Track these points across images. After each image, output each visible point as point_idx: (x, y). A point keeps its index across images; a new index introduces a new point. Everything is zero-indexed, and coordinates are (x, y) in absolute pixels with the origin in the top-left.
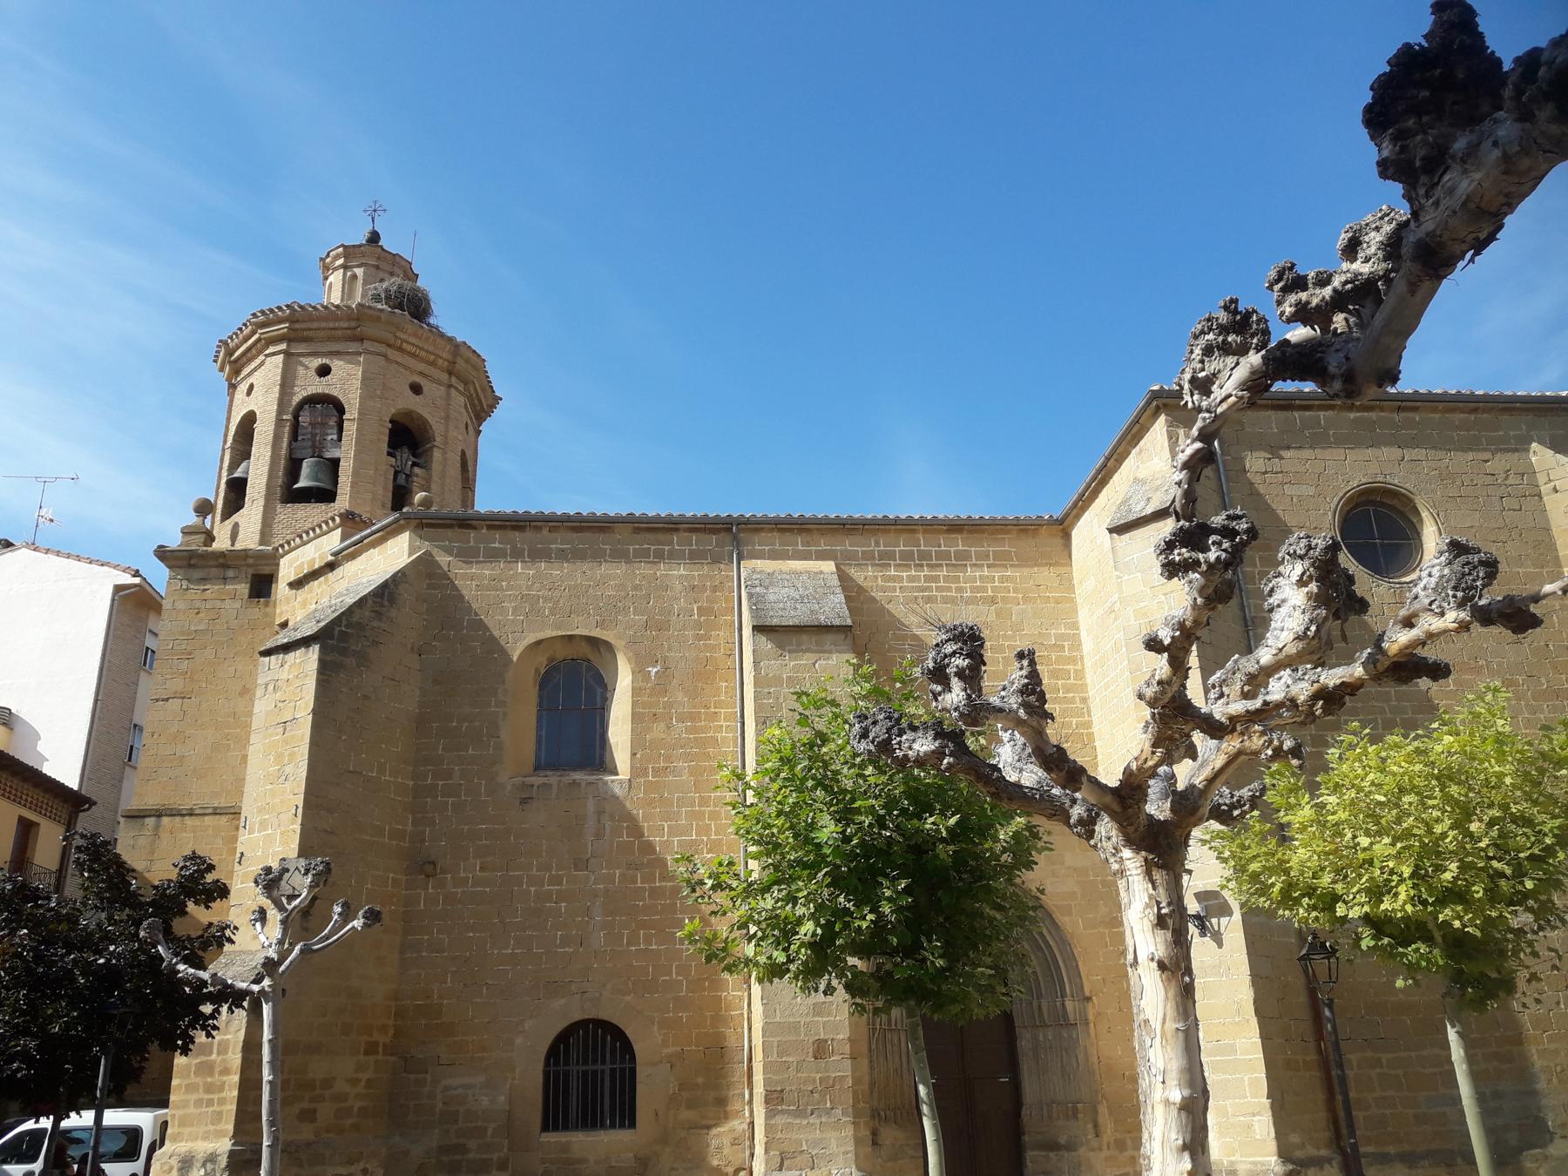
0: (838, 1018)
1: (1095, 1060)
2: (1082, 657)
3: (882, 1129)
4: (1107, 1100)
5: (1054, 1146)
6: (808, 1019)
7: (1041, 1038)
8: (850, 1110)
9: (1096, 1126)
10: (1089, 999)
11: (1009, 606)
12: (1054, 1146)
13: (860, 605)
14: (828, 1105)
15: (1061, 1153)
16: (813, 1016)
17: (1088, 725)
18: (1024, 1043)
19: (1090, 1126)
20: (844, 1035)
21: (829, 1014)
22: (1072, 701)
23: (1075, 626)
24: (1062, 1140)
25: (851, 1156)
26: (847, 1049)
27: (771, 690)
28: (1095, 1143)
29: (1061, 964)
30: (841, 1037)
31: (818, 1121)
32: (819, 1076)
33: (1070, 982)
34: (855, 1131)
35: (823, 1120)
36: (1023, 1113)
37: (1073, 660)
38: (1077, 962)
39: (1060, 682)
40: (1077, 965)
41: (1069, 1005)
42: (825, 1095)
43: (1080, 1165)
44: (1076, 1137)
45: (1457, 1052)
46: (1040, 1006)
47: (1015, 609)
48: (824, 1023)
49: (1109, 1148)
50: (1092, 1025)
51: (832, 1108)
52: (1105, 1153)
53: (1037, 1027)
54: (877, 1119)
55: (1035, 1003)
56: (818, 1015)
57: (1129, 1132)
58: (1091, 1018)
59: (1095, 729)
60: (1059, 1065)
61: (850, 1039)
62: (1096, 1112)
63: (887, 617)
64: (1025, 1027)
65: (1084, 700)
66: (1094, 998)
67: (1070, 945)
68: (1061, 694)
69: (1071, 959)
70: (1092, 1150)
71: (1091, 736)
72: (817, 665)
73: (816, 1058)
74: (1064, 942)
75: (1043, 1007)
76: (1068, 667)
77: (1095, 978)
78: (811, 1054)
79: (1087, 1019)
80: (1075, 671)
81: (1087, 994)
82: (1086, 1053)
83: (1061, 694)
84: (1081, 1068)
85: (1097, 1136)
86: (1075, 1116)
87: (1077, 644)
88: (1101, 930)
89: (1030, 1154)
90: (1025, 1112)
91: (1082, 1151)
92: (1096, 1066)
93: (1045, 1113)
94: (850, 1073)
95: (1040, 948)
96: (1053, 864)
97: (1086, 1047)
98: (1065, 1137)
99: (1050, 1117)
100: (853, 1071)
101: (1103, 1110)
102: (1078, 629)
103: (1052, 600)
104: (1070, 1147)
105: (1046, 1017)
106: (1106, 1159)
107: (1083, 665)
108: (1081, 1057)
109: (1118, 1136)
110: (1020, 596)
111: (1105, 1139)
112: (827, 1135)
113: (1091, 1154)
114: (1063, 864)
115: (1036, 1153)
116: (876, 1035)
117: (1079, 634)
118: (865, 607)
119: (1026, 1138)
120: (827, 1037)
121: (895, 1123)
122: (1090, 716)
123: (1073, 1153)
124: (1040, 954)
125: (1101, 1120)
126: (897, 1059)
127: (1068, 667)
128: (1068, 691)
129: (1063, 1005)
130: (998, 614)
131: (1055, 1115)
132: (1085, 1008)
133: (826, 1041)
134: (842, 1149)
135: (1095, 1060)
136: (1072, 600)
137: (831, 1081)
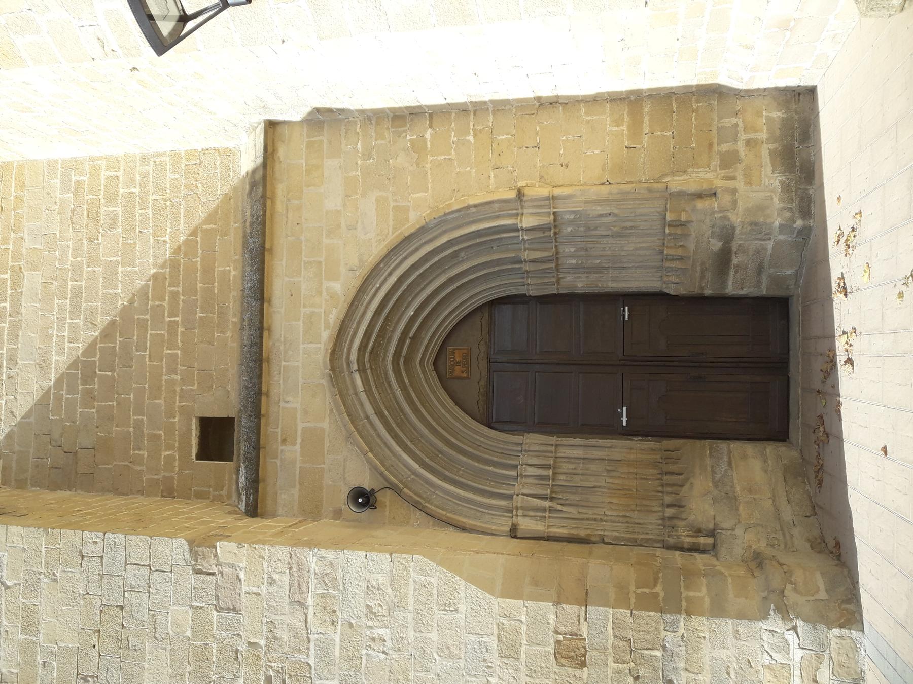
0: (523, 619)
1: (605, 190)
2: (92, 159)
3: (692, 517)
4: (664, 176)
5: (723, 260)
6: (523, 669)
7: (574, 262)
8: (668, 617)
9: (700, 196)
10: (520, 194)
11: (24, 252)
12: (723, 260)
13: (15, 457)
14: (658, 653)
15: (734, 249)
16: (518, 659)
17: (175, 155)
18: (580, 284)
19: (700, 204)
20: (548, 611)
21: (517, 632)
22: (145, 176)
23: (52, 165)
24: (716, 245)
25: (742, 626)
26: (571, 610)
27: (40, 661)
28: (726, 199)
29: (473, 228)
30: (552, 617)
31: (684, 674)
32: (611, 664)
33: (498, 217)
34: (701, 614)
35: (682, 665)
36: (672, 293)
37: (95, 171)
38: (468, 207)
39: (121, 191)
40: (475, 206)
41: (528, 222)
42: (643, 657)
43: (756, 224)
44: (713, 227)
45: (625, 419)
46: (531, 261)
47: (28, 244)
48: (531, 643)
49: (734, 178)
50: (557, 192)
51: (664, 648)
52: (740, 184)
53: (557, 265)
54: (676, 522)
55: (526, 267)
56: (516, 649)
57: (711, 145)
58: (545, 192)
59: (182, 147)
60: (610, 240)
61: (557, 603)
62: (680, 194)
63: (32, 419)
64: (558, 281)
65: (145, 159)
66: (520, 185)
67: (445, 215)
68: (137, 191)
69: (466, 213)
70: (735, 202)
71: (189, 154)
72: (9, 583)
73: (583, 664)
74: (444, 221)
75: (531, 258)
76: (103, 178)
77: (492, 180)
78: (578, 672)
79: (548, 198)
80: (108, 169)
81: (512, 195)
82: (597, 202)
83: (137, 191)
84: (616, 211)
85: (715, 194)
86: (683, 225)
87: (74, 165)
88: (428, 166)
89: (731, 289)
90: (671, 290)
91: (736, 219)
92: (614, 189)
93: (673, 264)
94: (610, 610)
95: (455, 255)
96: (339, 226)
97: (586, 202)
98: (713, 241)
99: (681, 259)
100: (606, 605)
101: (676, 183)
102: (56, 161)
103: (21, 193)
104: (727, 235)
105: (545, 254)
106: (749, 183)
107: (101, 158)
108: (600, 210)
109: (716, 162)
110: (13, 235)
111: (719, 183)
112: (707, 661)
113: (740, 204)
114: (338, 212)
115: (730, 282)
116: (559, 507)
117: (63, 160)
118: (17, 448)
119: (708, 292)
120: (552, 642)
121: (682, 486)
122: (163, 154)
123: (737, 232)
124: (462, 254)
125: (693, 188)
126: (594, 467)
127: (103, 178)
128: (133, 181)
129: (529, 230)
130: (34, 267)
131: (679, 252)
132: (532, 200)
133: (558, 642)
134: (731, 640)
135: (605, 190)
136: (21, 167)
137: (621, 644)
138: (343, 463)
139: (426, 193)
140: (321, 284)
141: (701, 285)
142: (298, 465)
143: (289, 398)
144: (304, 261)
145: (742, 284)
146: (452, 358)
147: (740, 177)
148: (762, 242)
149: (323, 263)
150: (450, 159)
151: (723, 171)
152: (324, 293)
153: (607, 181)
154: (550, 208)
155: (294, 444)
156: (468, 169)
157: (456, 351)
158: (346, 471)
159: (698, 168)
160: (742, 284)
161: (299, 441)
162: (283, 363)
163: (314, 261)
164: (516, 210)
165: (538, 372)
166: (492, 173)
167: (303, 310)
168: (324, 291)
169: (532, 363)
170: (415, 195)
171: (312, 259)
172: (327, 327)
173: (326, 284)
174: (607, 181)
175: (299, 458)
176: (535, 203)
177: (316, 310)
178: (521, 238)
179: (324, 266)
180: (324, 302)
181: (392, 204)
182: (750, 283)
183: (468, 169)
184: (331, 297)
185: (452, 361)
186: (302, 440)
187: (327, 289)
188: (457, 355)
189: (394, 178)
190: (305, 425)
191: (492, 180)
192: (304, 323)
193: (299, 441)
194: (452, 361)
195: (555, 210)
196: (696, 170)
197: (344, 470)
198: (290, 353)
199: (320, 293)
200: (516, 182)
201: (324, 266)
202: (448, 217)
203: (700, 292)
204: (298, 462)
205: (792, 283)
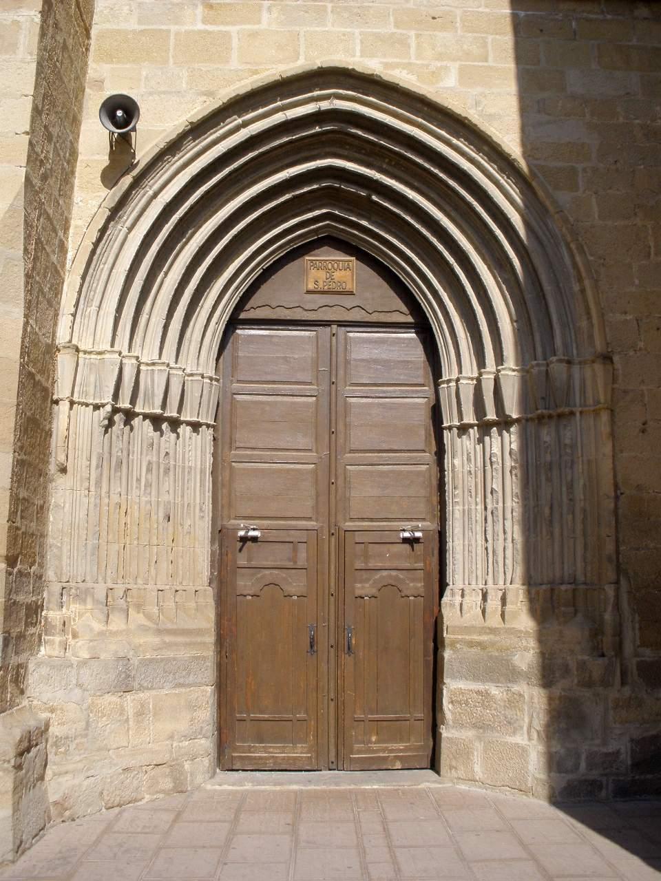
77: (620, 317)
138: (173, 90)
139: (599, 216)
140: (454, 60)
141: (457, 642)
142: (174, 28)
143: (275, 14)
144: (486, 38)
145: (460, 703)
146: (338, 266)
147: (627, 691)
148: (525, 728)
149: (485, 64)
150: (649, 254)
151: (635, 667)
152: (439, 64)
153: (622, 494)
154: (581, 406)
155: (204, 21)
156: (637, 282)
157: (348, 273)
158: (163, 96)
159: (640, 628)
160: (460, 703)
161: (210, 28)
162: (329, 6)
163: (488, 51)
164: (578, 354)
165: (318, 367)
166: (631, 317)
167: (412, 33)
168: (444, 63)
169: (337, 353)
170: (594, 200)
171: (490, 48)
172: (386, 65)
173: (454, 67)
174: (622, 494)
175: (184, 28)
176: (589, 383)
177: (413, 51)
178: (554, 359)
179: (480, 64)
180: (425, 62)
181: (580, 167)
182: (460, 714)
183: (637, 282)
184: (434, 72)
185: (333, 266)
186: (209, 33)
187: (446, 68)
188: (343, 272)
189: (617, 170)
190: (234, 35)
191: (620, 317)
192: (393, 34)
193: (210, 28)
194: (333, 266)
195: (578, 414)
196: (637, 626)
197: (164, 93)
198: (346, 15)
199: (440, 57)
200: (619, 353)
201: (480, 64)
202: (564, 248)
203: (447, 642)
204: (177, 27)
205: (461, 773)
